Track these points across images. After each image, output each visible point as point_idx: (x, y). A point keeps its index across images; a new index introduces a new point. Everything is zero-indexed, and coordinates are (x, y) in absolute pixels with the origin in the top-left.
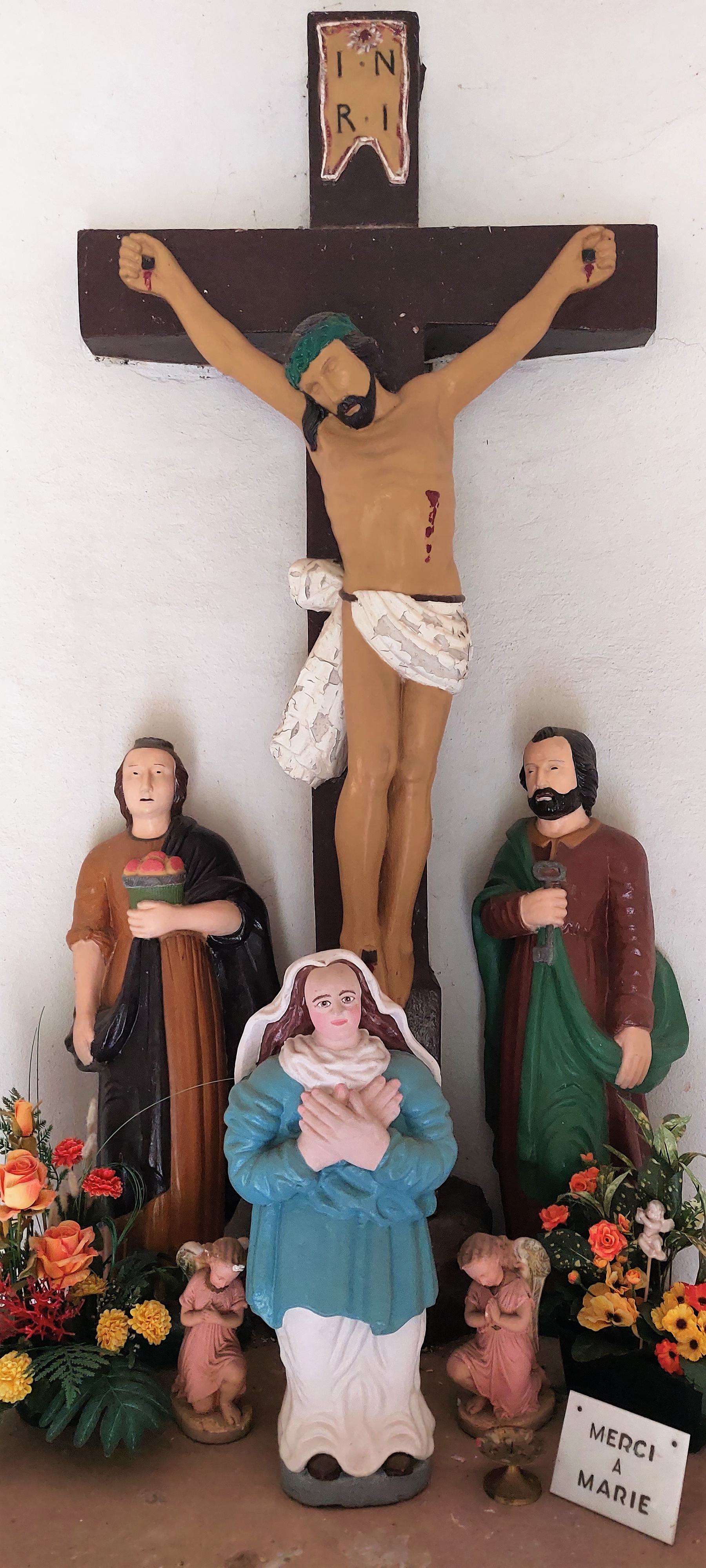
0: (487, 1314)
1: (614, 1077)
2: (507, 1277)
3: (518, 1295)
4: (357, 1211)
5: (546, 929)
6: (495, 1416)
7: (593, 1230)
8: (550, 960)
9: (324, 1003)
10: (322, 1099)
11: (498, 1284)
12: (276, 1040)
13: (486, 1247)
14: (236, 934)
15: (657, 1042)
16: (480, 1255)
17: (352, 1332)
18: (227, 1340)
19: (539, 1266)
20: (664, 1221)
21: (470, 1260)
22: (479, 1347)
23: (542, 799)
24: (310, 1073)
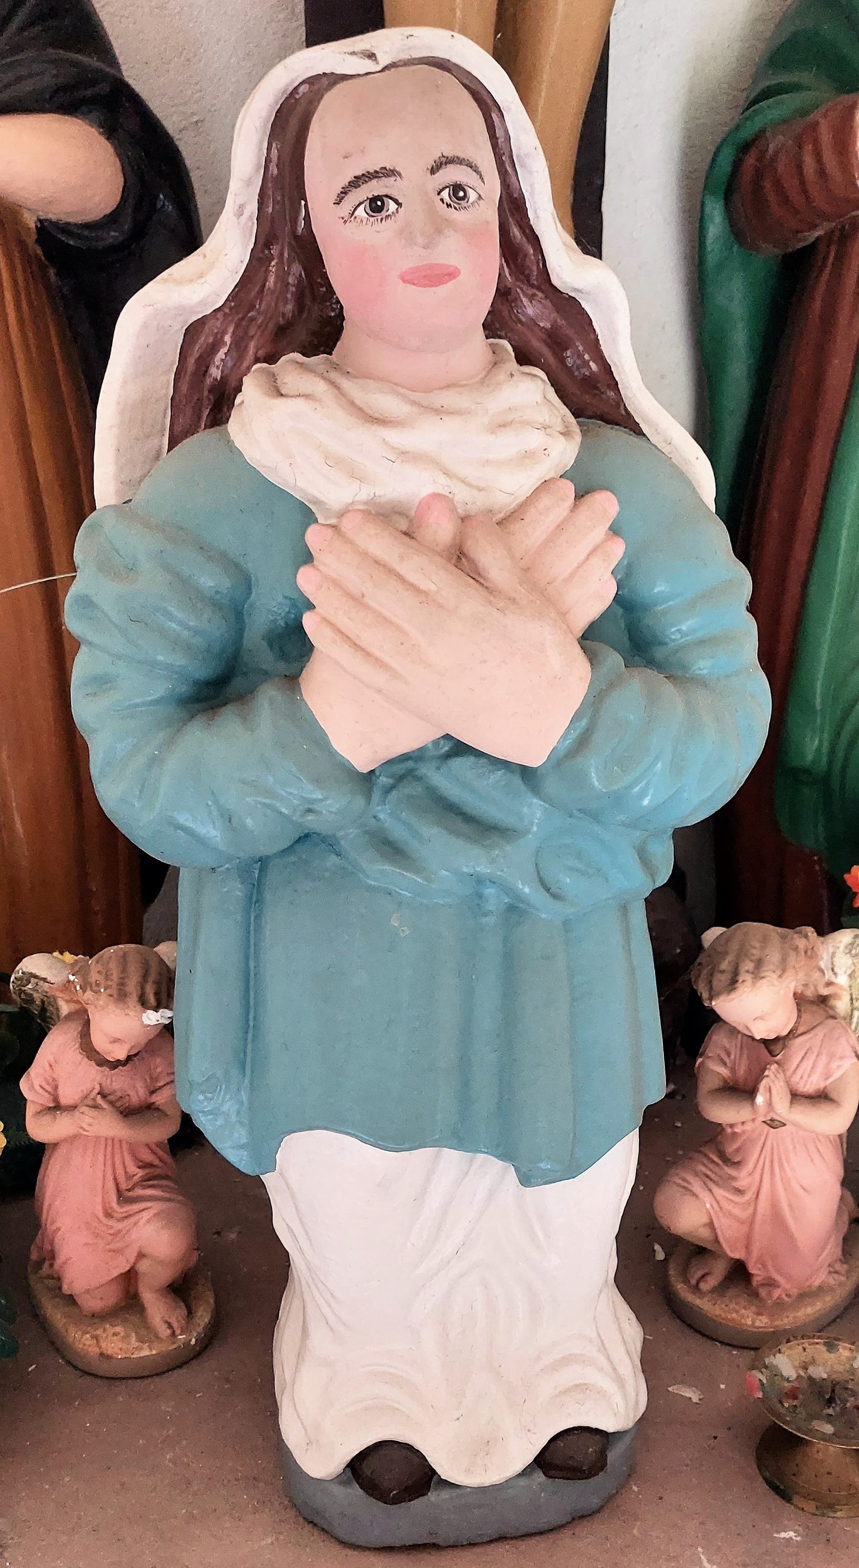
0: (760, 1099)
2: (805, 1017)
3: (831, 1057)
4: (479, 880)
6: (755, 1294)
9: (376, 205)
10: (380, 544)
11: (785, 1033)
12: (215, 373)
13: (773, 956)
14: (112, 219)
16: (757, 974)
17: (463, 1183)
18: (144, 1165)
21: (733, 984)
22: (726, 1160)
24: (334, 461)
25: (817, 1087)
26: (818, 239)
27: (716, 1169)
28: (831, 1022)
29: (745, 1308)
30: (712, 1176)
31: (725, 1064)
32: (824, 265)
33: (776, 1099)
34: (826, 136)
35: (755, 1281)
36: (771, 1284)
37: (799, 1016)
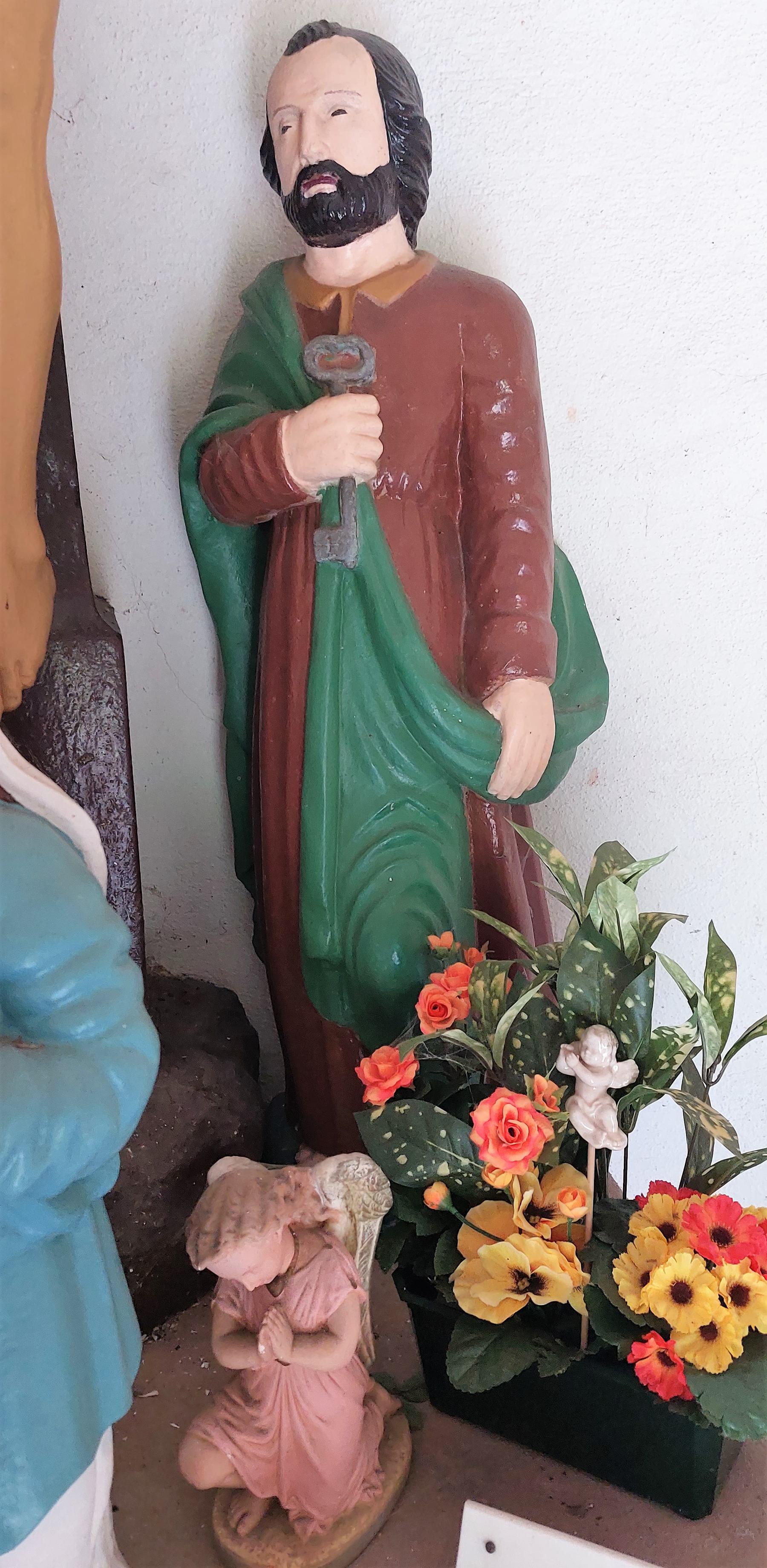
0: (262, 1348)
1: (487, 780)
2: (303, 1249)
3: (329, 1289)
5: (342, 487)
7: (482, 1114)
8: (351, 557)
11: (284, 1270)
13: (253, 1210)
15: (562, 702)
16: (238, 1234)
19: (367, 1200)
20: (617, 1066)
23: (314, 190)
25: (319, 1321)
26: (274, 517)
27: (239, 1413)
28: (327, 1251)
29: (280, 1551)
30: (235, 1421)
31: (235, 1305)
32: (280, 541)
33: (276, 1345)
34: (258, 447)
35: (292, 1515)
36: (305, 1518)
37: (297, 1251)
